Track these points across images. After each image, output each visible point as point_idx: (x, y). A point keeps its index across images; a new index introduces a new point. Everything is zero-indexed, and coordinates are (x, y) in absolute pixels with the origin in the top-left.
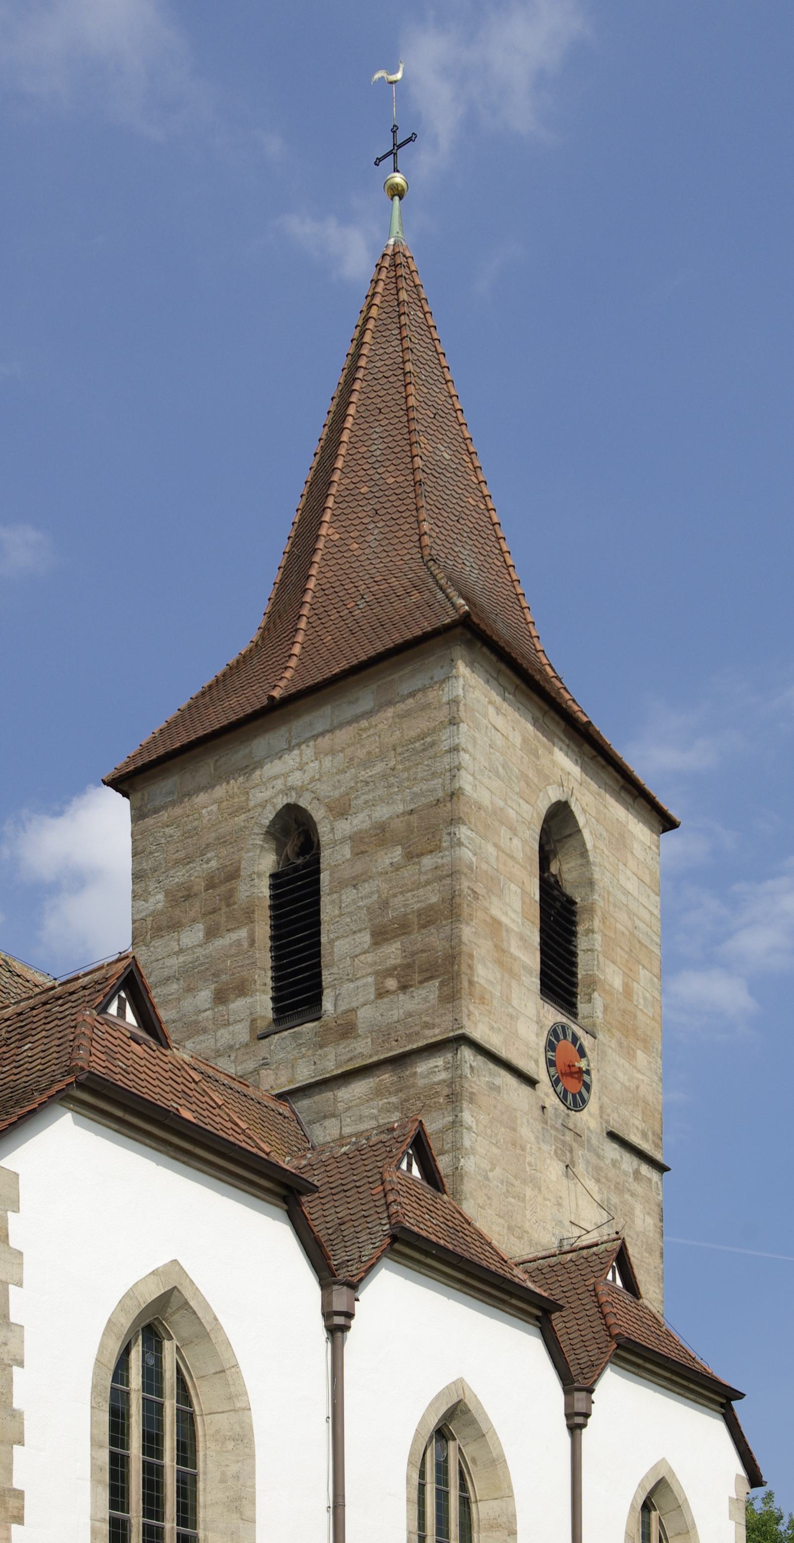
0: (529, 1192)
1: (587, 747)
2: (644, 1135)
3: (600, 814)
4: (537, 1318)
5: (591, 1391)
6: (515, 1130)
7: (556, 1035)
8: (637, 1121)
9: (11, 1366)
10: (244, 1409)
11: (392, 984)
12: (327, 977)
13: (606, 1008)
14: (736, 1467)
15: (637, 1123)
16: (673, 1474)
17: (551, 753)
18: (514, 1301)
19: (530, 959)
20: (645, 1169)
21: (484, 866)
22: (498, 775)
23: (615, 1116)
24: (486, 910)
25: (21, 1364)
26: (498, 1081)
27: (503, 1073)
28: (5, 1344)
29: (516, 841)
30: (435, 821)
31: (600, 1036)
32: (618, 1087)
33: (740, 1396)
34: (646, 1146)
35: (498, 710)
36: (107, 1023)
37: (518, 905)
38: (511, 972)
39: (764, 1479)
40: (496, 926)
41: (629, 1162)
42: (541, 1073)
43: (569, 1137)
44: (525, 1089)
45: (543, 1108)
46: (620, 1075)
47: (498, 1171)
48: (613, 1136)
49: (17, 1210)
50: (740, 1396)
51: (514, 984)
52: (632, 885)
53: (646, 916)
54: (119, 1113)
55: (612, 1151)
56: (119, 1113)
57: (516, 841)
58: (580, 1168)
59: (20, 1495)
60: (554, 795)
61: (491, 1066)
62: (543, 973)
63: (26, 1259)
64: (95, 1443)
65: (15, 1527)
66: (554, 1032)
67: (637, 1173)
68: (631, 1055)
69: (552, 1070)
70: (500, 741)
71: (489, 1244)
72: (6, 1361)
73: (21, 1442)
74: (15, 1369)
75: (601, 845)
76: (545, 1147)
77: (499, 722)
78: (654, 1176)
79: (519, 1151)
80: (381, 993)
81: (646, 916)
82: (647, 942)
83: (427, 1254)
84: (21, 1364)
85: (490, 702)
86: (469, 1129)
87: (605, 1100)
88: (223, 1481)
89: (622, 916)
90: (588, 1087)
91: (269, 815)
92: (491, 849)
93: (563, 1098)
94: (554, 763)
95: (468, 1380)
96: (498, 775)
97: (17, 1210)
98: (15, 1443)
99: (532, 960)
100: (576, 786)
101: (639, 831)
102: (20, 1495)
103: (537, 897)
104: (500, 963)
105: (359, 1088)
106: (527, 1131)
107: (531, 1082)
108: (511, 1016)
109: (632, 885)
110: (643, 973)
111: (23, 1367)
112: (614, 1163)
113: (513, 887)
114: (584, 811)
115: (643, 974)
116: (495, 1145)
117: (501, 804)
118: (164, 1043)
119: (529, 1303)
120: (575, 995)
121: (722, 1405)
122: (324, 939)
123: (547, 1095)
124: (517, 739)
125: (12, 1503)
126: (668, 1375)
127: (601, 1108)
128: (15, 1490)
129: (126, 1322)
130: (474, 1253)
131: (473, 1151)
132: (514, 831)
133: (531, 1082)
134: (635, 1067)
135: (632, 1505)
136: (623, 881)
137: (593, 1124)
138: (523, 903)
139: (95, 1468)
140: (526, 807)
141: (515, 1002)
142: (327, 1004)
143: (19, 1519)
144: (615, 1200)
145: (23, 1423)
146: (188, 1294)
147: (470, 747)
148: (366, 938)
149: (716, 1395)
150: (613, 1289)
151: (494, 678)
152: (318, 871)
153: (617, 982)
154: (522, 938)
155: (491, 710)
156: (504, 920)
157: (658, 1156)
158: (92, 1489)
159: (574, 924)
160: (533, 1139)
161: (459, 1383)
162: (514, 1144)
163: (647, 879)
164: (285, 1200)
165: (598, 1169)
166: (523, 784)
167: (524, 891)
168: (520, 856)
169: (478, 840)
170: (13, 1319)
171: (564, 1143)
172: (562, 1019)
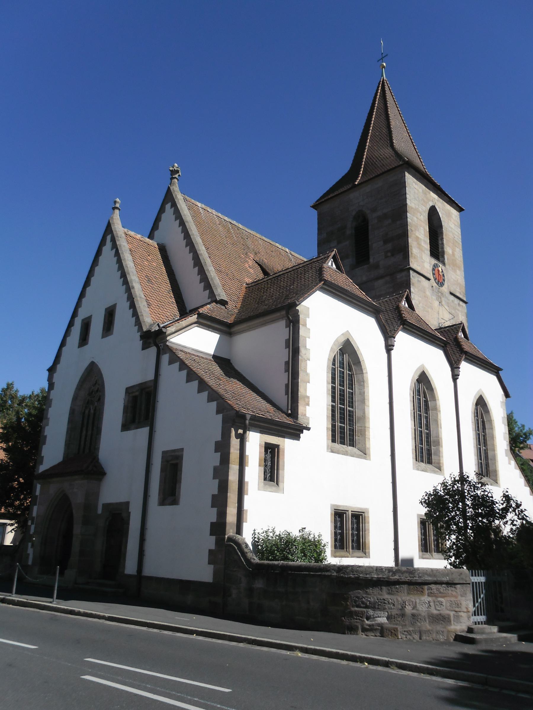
0: (430, 310)
1: (439, 192)
2: (460, 293)
4: (443, 347)
6: (425, 293)
7: (435, 266)
8: (458, 290)
11: (389, 254)
12: (371, 253)
13: (448, 259)
16: (483, 393)
17: (430, 193)
19: (426, 246)
20: (461, 303)
21: (414, 223)
24: (415, 234)
25: (309, 360)
26: (420, 280)
30: (400, 211)
31: (447, 266)
33: (501, 370)
34: (461, 296)
36: (329, 268)
37: (423, 233)
38: (422, 250)
40: (417, 238)
41: (457, 301)
42: (431, 277)
43: (440, 294)
47: (421, 305)
48: (451, 294)
49: (309, 318)
50: (501, 370)
51: (423, 253)
52: (452, 226)
53: (457, 234)
54: (334, 291)
55: (452, 297)
56: (334, 291)
58: (443, 303)
59: (308, 397)
60: (431, 204)
61: (418, 275)
62: (430, 250)
64: (328, 383)
65: (307, 407)
66: (434, 266)
67: (459, 304)
68: (455, 271)
71: (455, 325)
73: (309, 382)
75: (444, 216)
76: (433, 297)
77: (416, 187)
78: (464, 305)
80: (386, 257)
81: (457, 234)
83: (413, 328)
84: (309, 360)
85: (414, 182)
88: (360, 394)
89: (451, 234)
90: (444, 280)
91: (354, 213)
92: (415, 219)
93: (438, 284)
94: (431, 196)
95: (425, 365)
97: (309, 318)
99: (428, 247)
101: (455, 213)
104: (419, 248)
105: (381, 282)
106: (428, 293)
107: (429, 279)
109: (452, 226)
110: (457, 250)
112: (453, 301)
113: (422, 228)
115: (457, 250)
117: (417, 207)
119: (441, 342)
120: (439, 256)
121: (496, 372)
122: (370, 243)
124: (421, 190)
125: (306, 400)
127: (448, 286)
129: (337, 349)
130: (424, 327)
132: (421, 213)
133: (429, 279)
139: (328, 390)
140: (424, 208)
142: (371, 260)
143: (308, 404)
144: (453, 312)
148: (381, 243)
149: (495, 370)
150: (461, 338)
151: (414, 176)
152: (368, 226)
154: (424, 241)
156: (420, 237)
157: (465, 299)
159: (438, 237)
161: (423, 366)
162: (425, 297)
163: (456, 224)
164: (375, 313)
165: (448, 303)
168: (423, 220)
170: (307, 347)
171: (438, 296)
172: (436, 262)
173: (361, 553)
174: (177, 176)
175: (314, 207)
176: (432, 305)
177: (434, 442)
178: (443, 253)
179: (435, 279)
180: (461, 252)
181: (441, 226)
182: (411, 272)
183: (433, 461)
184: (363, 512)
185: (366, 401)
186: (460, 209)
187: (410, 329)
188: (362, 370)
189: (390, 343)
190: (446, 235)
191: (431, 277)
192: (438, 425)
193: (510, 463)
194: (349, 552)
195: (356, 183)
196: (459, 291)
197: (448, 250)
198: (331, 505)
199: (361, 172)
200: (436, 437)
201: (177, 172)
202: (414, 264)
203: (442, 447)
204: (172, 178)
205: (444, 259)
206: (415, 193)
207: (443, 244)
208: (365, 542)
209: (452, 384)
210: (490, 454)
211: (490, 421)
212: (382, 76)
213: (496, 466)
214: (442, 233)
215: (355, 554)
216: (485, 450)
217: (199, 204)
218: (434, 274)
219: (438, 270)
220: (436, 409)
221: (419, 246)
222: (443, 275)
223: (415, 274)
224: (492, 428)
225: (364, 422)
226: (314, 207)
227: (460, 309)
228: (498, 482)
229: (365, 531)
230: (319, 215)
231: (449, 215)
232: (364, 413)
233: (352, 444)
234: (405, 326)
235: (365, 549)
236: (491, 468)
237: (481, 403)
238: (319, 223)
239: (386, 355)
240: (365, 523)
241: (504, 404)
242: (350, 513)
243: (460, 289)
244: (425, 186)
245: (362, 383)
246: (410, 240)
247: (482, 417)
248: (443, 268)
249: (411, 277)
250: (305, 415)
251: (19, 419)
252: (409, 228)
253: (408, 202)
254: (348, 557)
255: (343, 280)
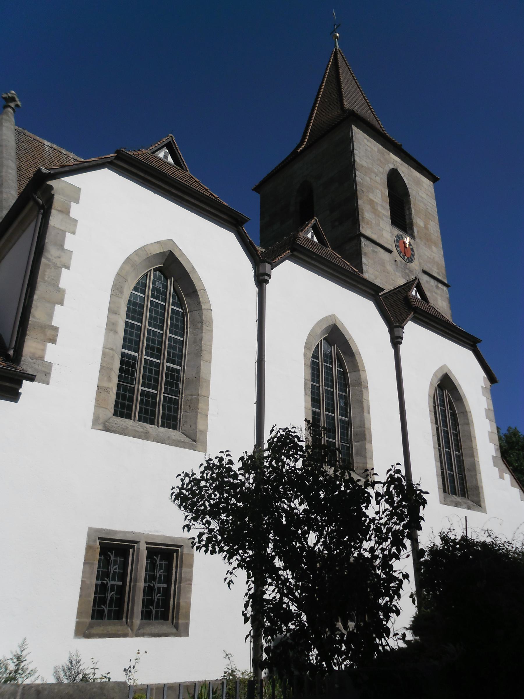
2: (439, 274)
3: (410, 175)
4: (373, 295)
5: (403, 328)
6: (384, 267)
9: (61, 268)
10: (208, 309)
13: (418, 232)
14: (482, 374)
15: (435, 270)
17: (389, 154)
18: (360, 286)
19: (385, 211)
20: (440, 285)
21: (366, 183)
22: (369, 158)
23: (426, 266)
24: (367, 196)
26: (376, 250)
27: (378, 247)
28: (59, 258)
29: (377, 178)
31: (417, 240)
32: (426, 257)
33: (479, 341)
35: (368, 141)
37: (380, 196)
39: (497, 379)
40: (371, 202)
42: (394, 249)
44: (387, 254)
45: (395, 261)
46: (426, 253)
48: (425, 272)
50: (479, 341)
51: (380, 220)
52: (424, 196)
57: (377, 178)
60: (391, 166)
61: (373, 245)
63: (79, 224)
65: (49, 345)
66: (398, 236)
67: (437, 287)
69: (398, 249)
70: (369, 149)
72: (59, 265)
73: (61, 304)
74: (63, 269)
76: (398, 274)
77: (369, 144)
78: (445, 288)
79: (386, 274)
82: (432, 213)
84: (68, 268)
85: (365, 138)
86: (365, 264)
87: (421, 261)
88: (195, 342)
90: (413, 256)
92: (368, 179)
93: (404, 259)
94: (391, 158)
95: (337, 315)
96: (369, 158)
98: (57, 304)
100: (399, 165)
101: (426, 182)
102: (56, 329)
103: (388, 195)
107: (390, 252)
108: (380, 230)
109: (424, 196)
111: (69, 269)
114: (403, 172)
116: (377, 271)
117: (371, 166)
118: (185, 169)
119: (367, 287)
120: (406, 228)
121: (472, 346)
123: (397, 257)
125: (49, 332)
126: (442, 328)
127: (420, 263)
128: (53, 326)
131: (367, 272)
133: (390, 252)
134: (432, 251)
135: (431, 383)
136: (420, 194)
137: (417, 268)
138: (382, 196)
140: (381, 169)
141: (381, 226)
143: (53, 341)
145: (64, 295)
146: (177, 254)
147: (358, 149)
153: (422, 224)
154: (382, 206)
155: (365, 141)
156: (375, 200)
157: (446, 282)
158: (106, 333)
160: (392, 270)
162: (384, 271)
163: (430, 194)
166: (379, 162)
167: (382, 193)
169: (363, 176)
170: (66, 247)
171: (406, 273)
173: (166, 627)
174: (12, 105)
175: (257, 189)
176: (382, 269)
177: (357, 435)
178: (412, 224)
179: (400, 253)
180: (438, 226)
181: (406, 194)
182: (362, 239)
183: (355, 465)
184: (180, 546)
185: (204, 353)
186: (434, 179)
187: (307, 259)
188: (199, 304)
189: (261, 271)
190: (414, 205)
191: (394, 249)
192: (363, 408)
193: (502, 477)
194: (131, 626)
195: (299, 151)
196: (437, 271)
197: (418, 222)
198: (90, 529)
199: (306, 140)
200: (360, 427)
201: (13, 99)
202: (365, 230)
203: (371, 442)
204: (6, 107)
205: (413, 231)
206: (366, 150)
207: (410, 214)
208: (179, 604)
209: (392, 351)
210: (467, 461)
211: (465, 413)
212: (335, 46)
213: (476, 480)
214: (409, 202)
215: (148, 630)
216: (458, 457)
217: (46, 143)
218: (397, 246)
219: (404, 243)
220: (361, 385)
221: (374, 210)
222: (412, 250)
223: (368, 243)
224: (468, 423)
225: (197, 389)
226: (257, 189)
227: (438, 292)
228: (482, 505)
229: (180, 582)
230: (262, 198)
231: (418, 183)
232: (198, 372)
233: (171, 421)
234: (295, 253)
235: (178, 618)
236: (469, 484)
237: (446, 389)
238: (262, 207)
239: (255, 290)
240: (181, 567)
241: (489, 391)
242: (143, 547)
243: (438, 269)
244: (382, 145)
245: (199, 325)
246: (360, 202)
247: (452, 408)
248: (412, 241)
249: (363, 245)
250: (42, 358)
251: (393, 571)
252: (358, 188)
253: (357, 158)
254: (125, 635)
255: (254, 237)
